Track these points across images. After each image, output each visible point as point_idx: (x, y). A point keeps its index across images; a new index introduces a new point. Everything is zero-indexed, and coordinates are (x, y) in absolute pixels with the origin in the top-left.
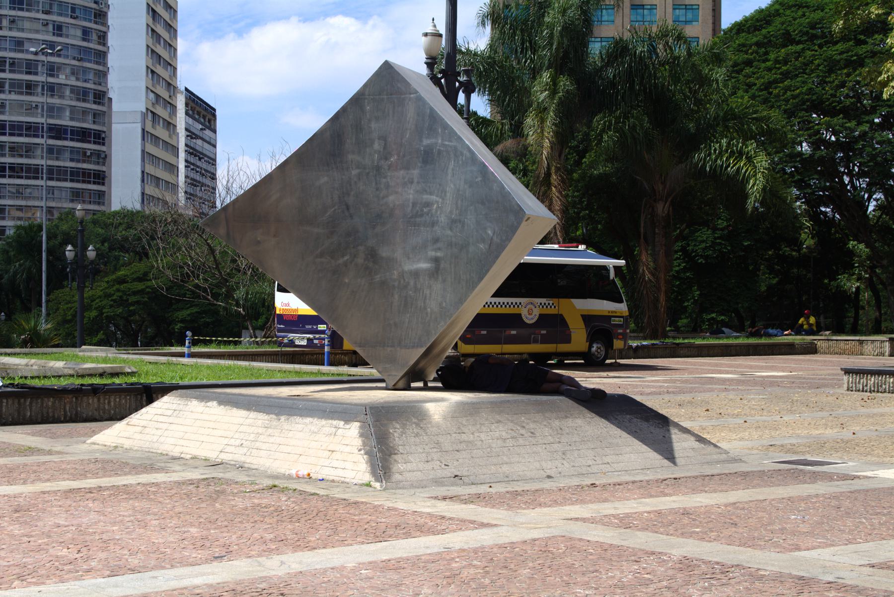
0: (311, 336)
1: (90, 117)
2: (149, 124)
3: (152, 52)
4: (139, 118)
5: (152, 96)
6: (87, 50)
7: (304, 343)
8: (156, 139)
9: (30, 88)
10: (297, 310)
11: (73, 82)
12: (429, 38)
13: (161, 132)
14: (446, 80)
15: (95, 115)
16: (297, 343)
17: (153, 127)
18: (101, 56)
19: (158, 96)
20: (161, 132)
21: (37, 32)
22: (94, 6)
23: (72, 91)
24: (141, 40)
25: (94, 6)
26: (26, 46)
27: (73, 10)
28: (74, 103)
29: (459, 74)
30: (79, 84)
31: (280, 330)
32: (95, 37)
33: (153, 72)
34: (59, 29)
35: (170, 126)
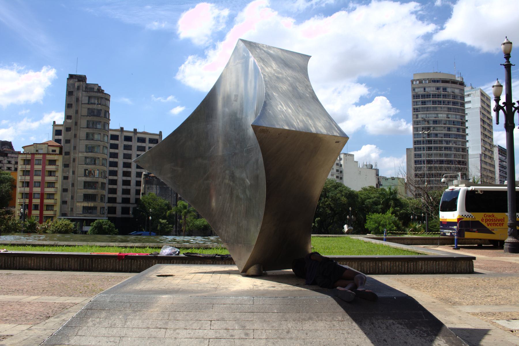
0: (451, 231)
1: (461, 157)
2: (483, 159)
3: (483, 134)
4: (479, 156)
5: (484, 148)
6: (459, 135)
7: (449, 234)
8: (486, 163)
9: (440, 149)
10: (446, 219)
11: (454, 145)
12: (495, 88)
13: (488, 160)
14: (506, 108)
15: (462, 156)
16: (447, 234)
17: (485, 158)
18: (464, 136)
19: (486, 148)
20: (488, 160)
21: (442, 130)
22: (460, 120)
23: (454, 149)
24: (479, 130)
25: (460, 120)
26: (439, 135)
27: (454, 122)
28: (455, 152)
29: (514, 104)
30: (456, 146)
31: (442, 229)
32: (461, 130)
33: (484, 140)
34: (449, 129)
35: (491, 158)
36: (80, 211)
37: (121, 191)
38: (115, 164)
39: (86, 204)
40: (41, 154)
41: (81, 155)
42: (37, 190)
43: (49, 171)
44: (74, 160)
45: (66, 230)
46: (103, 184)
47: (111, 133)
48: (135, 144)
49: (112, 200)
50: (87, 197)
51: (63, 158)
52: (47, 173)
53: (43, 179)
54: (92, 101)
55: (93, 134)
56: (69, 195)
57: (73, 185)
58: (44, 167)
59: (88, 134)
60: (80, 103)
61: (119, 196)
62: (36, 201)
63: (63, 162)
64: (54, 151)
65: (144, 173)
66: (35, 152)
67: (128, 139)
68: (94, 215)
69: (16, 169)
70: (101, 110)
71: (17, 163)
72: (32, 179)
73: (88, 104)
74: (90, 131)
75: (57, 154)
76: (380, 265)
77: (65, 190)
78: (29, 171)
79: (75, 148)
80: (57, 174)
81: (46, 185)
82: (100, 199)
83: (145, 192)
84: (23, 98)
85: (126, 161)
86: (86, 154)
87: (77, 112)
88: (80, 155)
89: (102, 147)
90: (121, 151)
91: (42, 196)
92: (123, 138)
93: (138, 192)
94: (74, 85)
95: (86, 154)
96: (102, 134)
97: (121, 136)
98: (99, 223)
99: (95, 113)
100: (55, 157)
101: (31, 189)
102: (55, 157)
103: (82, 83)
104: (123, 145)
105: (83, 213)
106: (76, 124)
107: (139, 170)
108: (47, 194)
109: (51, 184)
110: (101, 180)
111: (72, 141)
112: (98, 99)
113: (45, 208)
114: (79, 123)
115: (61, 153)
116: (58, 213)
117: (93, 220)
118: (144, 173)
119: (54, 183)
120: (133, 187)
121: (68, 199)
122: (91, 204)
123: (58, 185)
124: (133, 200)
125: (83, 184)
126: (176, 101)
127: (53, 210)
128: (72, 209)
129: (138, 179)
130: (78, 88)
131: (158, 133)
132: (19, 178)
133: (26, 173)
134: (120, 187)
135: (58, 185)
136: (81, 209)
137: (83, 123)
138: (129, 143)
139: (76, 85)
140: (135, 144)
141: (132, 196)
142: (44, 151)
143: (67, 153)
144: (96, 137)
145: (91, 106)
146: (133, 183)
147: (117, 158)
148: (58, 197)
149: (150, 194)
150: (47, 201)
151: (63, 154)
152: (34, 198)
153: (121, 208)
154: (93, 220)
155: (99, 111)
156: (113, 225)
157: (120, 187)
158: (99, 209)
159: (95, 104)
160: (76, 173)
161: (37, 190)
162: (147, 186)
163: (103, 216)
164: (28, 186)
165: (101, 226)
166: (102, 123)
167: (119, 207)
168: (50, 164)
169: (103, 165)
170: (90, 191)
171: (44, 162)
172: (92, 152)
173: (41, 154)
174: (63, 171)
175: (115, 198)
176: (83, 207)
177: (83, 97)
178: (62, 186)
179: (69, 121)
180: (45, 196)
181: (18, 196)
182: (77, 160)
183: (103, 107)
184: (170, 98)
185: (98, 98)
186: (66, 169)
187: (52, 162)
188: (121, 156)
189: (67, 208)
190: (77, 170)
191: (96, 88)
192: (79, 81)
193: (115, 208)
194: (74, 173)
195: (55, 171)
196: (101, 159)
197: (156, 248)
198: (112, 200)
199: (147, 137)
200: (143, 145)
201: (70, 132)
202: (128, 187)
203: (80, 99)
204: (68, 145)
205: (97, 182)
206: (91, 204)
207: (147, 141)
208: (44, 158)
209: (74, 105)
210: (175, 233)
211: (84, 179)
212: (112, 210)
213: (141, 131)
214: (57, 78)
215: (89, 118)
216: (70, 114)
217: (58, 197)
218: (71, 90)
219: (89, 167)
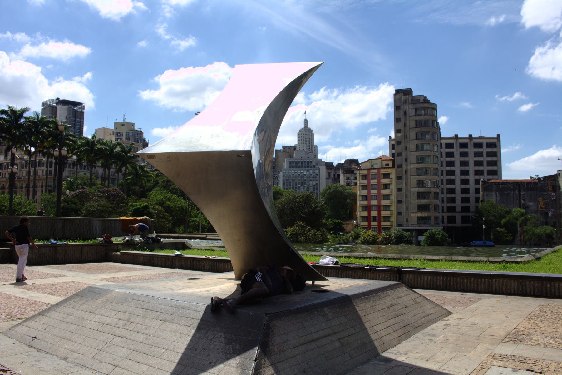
36: (415, 221)
37: (460, 199)
38: (452, 173)
39: (420, 215)
40: (375, 169)
41: (412, 167)
42: (374, 203)
43: (384, 184)
44: (406, 172)
45: (373, 240)
46: (436, 194)
47: (443, 142)
48: (471, 150)
49: (451, 209)
50: (421, 208)
51: (396, 171)
52: (382, 187)
53: (379, 192)
54: (418, 113)
55: (422, 145)
56: (404, 206)
57: (407, 196)
58: (379, 181)
59: (417, 146)
60: (408, 116)
61: (458, 204)
62: (374, 213)
63: (396, 175)
64: (387, 165)
65: (482, 180)
66: (371, 167)
67: (464, 145)
68: (428, 225)
69: (355, 184)
70: (428, 120)
71: (355, 178)
72: (369, 192)
73: (415, 116)
74: (419, 142)
75: (390, 168)
76: (548, 286)
77: (400, 202)
78: (366, 185)
79: (406, 160)
80: (392, 187)
81: (382, 198)
82: (433, 208)
83: (484, 199)
84: (367, 119)
85: (464, 168)
86: (417, 166)
87: (405, 125)
88: (412, 166)
89: (432, 157)
90: (457, 159)
91: (379, 208)
92: (458, 145)
93: (477, 200)
94: (400, 99)
95: (417, 166)
96: (431, 144)
97: (456, 144)
98: (432, 233)
99: (423, 125)
100: (389, 171)
101: (369, 203)
102: (389, 171)
103: (407, 96)
104: (459, 153)
105: (418, 223)
106: (405, 136)
107: (477, 177)
108: (384, 206)
109: (387, 197)
110: (434, 190)
111: (403, 154)
112: (424, 110)
113: (382, 219)
114: (408, 136)
115: (393, 166)
116: (394, 224)
117: (426, 230)
118: (482, 180)
119: (389, 195)
120: (472, 195)
121: (403, 210)
122: (425, 214)
123: (393, 197)
124: (472, 209)
125: (416, 194)
126: (524, 97)
127: (389, 221)
128: (407, 220)
129: (477, 186)
130: (405, 102)
131: (496, 136)
132: (359, 192)
133: (364, 187)
134: (458, 196)
135: (393, 197)
136: (416, 219)
137: (412, 135)
138: (465, 150)
139: (402, 99)
140: (471, 150)
141: (472, 205)
142: (378, 166)
143: (400, 166)
144: (426, 147)
145: (418, 118)
146: (472, 191)
147: (454, 166)
148: (393, 208)
149: (488, 201)
150: (384, 213)
151: (396, 167)
152: (373, 210)
153: (460, 217)
154: (426, 230)
155: (426, 122)
156: (445, 234)
157: (458, 196)
158: (433, 218)
159: (421, 115)
160: (409, 184)
161: (374, 203)
162: (486, 193)
163: (437, 225)
164: (366, 200)
165: (434, 235)
166: (431, 133)
167: (458, 216)
168: (384, 178)
169: (434, 174)
170: (423, 202)
171: (378, 176)
172: (422, 163)
173: (375, 169)
174: (397, 184)
175: (454, 208)
176: (418, 217)
177: (410, 109)
178: (397, 197)
179: (399, 135)
180: (382, 208)
181: (358, 209)
182: (409, 172)
183: (430, 116)
184: (516, 95)
185: (424, 109)
186: (399, 181)
187: (387, 176)
188: (457, 164)
189: (403, 219)
190: (409, 181)
191: (422, 99)
192: (405, 94)
193: (455, 217)
194: (407, 184)
195: (389, 184)
196: (432, 169)
197: (360, 258)
198: (451, 209)
199: (484, 142)
200: (480, 150)
201: (400, 146)
202: (467, 195)
203: (407, 112)
204: (400, 158)
205: (430, 192)
206: (425, 214)
207: (484, 145)
208: (379, 172)
209: (402, 119)
210: (519, 243)
211: (417, 190)
212: (452, 220)
213: (477, 136)
214: (96, 97)
215: (418, 130)
216: (399, 128)
217: (393, 208)
218: (399, 104)
219: (421, 177)
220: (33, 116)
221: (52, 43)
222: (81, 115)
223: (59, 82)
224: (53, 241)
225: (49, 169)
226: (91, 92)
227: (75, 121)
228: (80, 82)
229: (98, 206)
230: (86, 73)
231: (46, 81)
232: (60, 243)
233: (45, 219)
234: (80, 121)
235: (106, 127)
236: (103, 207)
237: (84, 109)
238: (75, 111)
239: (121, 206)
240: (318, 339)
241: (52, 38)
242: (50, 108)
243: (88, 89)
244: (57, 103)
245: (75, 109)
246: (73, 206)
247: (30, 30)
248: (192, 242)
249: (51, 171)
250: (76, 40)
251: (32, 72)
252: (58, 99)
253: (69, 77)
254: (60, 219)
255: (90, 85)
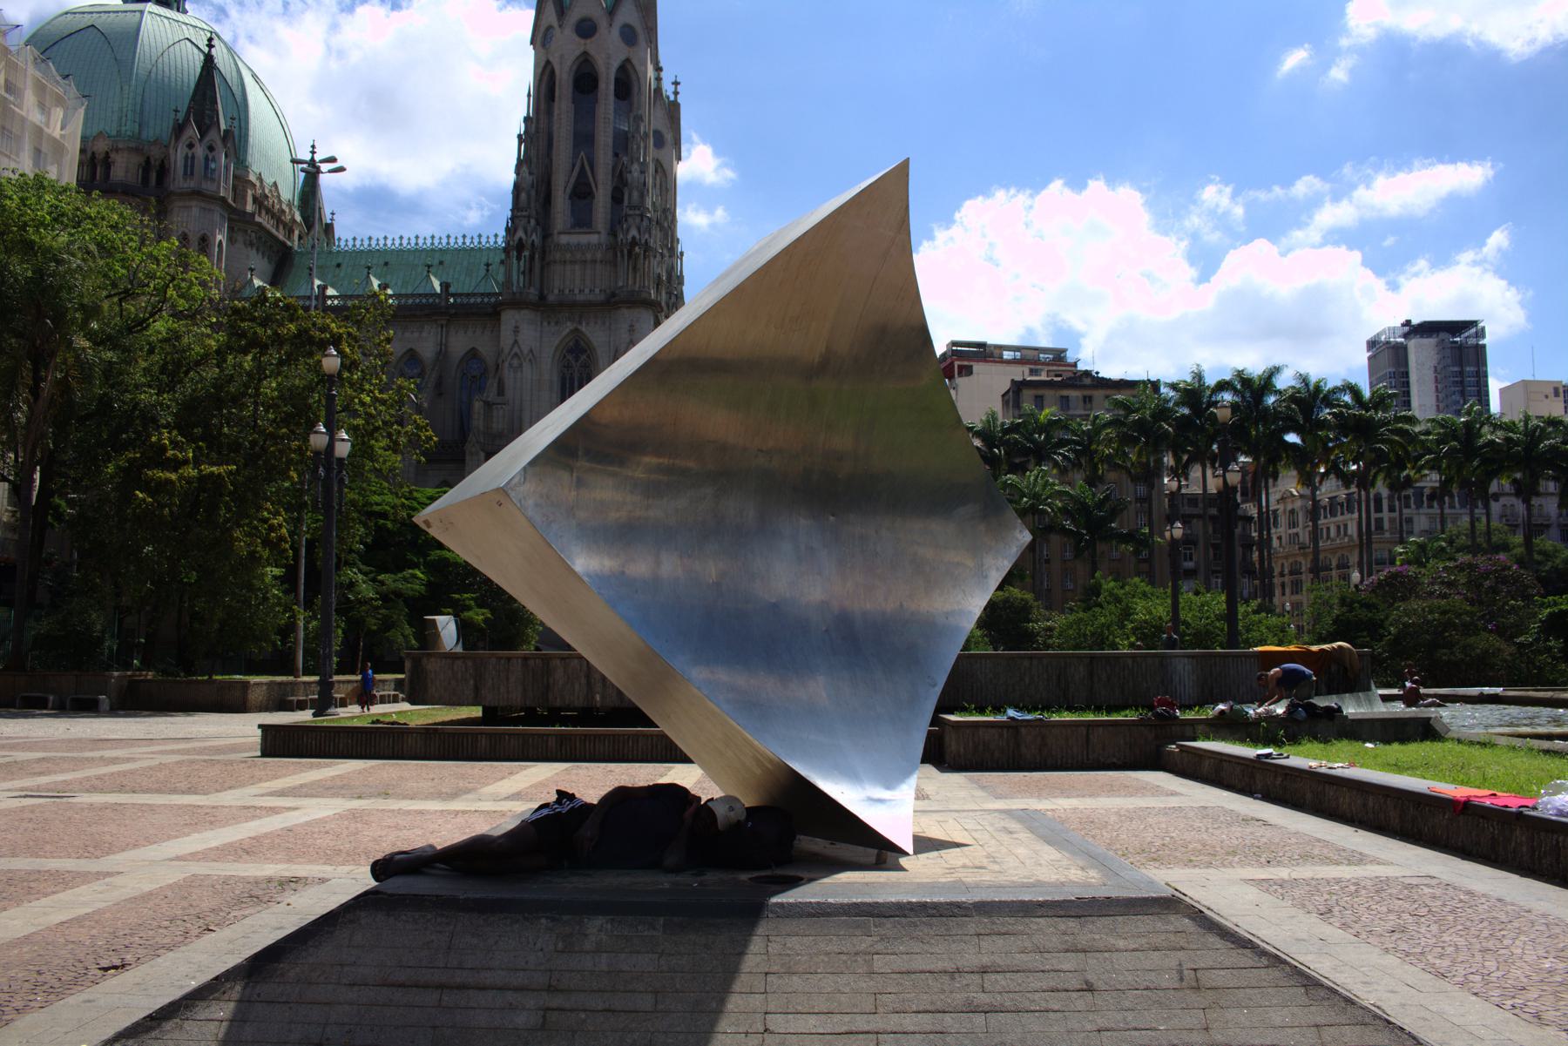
214: (1530, 293)
220: (1293, 383)
221: (1381, 181)
222: (1478, 355)
223: (1416, 275)
224: (1011, 713)
225: (1374, 516)
226: (1510, 283)
227: (1461, 373)
228: (1475, 263)
229: (1431, 612)
230: (1489, 235)
231: (1380, 285)
232: (1029, 717)
233: (1040, 657)
234: (1478, 372)
235: (1529, 378)
236: (1444, 613)
237: (1483, 336)
238: (1460, 348)
239: (1513, 607)
240: (463, 987)
241: (1378, 168)
242: (1389, 355)
243: (1502, 278)
244: (1405, 336)
245: (1457, 345)
246: (1364, 614)
247: (1325, 166)
248: (1447, 715)
249: (1379, 521)
250: (1447, 149)
251: (1346, 271)
252: (1408, 323)
253: (1442, 260)
254: (1079, 657)
255: (1508, 268)
